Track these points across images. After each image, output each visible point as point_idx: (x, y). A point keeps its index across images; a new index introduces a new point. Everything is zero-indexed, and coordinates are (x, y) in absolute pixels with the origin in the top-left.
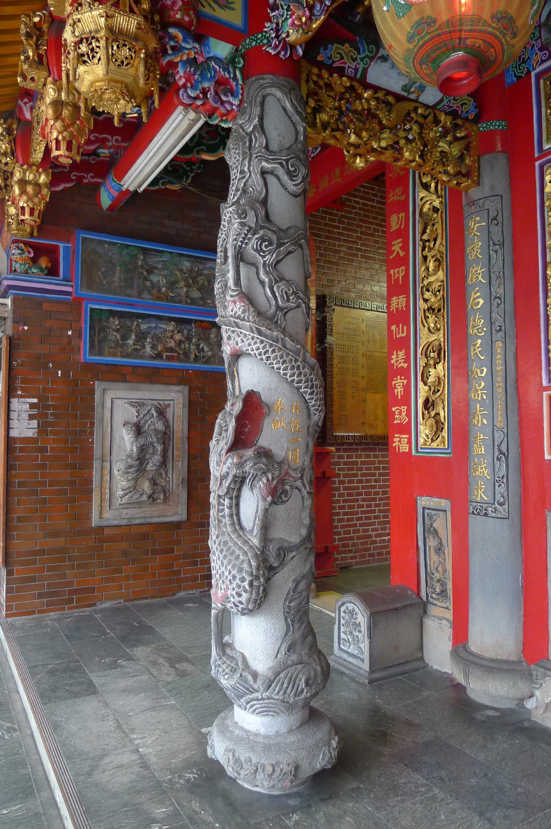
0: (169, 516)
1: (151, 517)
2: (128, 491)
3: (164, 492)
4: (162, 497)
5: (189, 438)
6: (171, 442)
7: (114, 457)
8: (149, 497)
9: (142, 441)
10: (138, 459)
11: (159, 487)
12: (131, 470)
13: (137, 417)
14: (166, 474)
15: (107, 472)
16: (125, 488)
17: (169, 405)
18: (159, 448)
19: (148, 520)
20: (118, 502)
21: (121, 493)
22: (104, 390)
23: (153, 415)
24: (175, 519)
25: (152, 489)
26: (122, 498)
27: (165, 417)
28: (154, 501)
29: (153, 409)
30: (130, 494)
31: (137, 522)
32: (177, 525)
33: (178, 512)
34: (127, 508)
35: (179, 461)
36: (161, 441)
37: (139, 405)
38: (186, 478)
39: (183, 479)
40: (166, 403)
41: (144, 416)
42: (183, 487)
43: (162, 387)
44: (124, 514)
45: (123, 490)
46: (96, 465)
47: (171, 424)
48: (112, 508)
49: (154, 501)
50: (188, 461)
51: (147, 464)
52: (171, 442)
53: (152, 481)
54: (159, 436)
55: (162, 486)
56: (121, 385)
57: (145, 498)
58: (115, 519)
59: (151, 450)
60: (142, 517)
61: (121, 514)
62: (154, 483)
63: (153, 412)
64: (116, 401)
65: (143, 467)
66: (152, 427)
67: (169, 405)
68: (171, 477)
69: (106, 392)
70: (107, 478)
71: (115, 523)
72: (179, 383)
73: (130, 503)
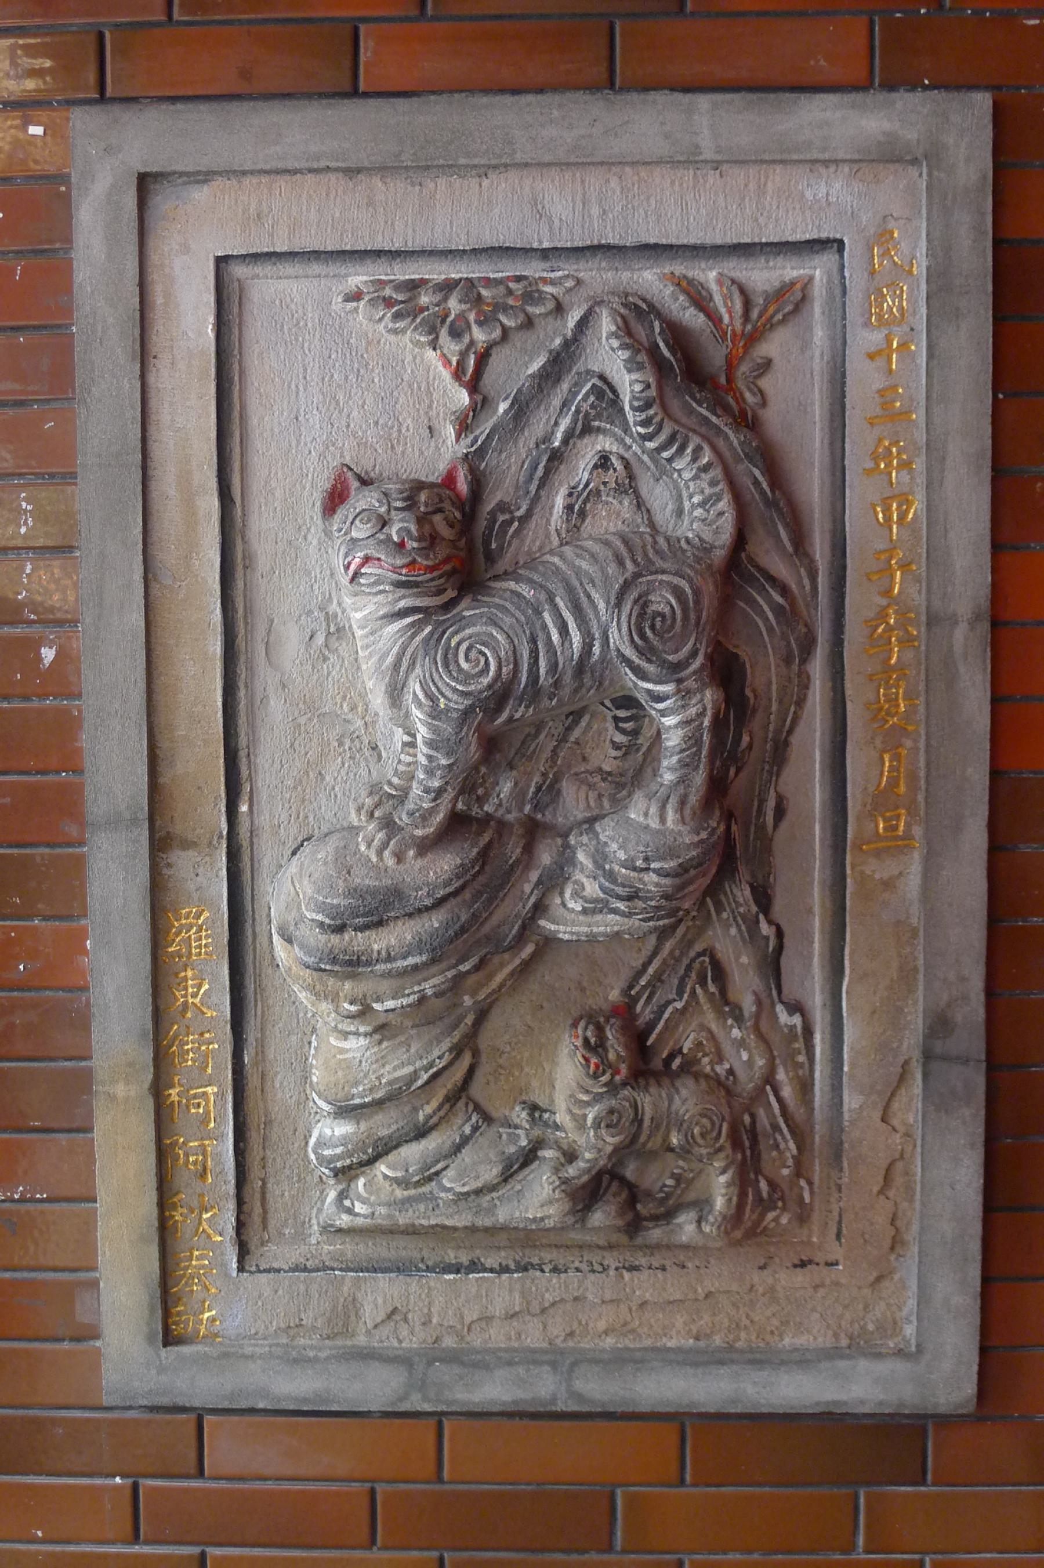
0: (803, 1360)
1: (621, 1361)
2: (391, 1119)
3: (746, 1146)
4: (719, 1187)
5: (1000, 621)
6: (818, 668)
7: (271, 807)
8: (585, 1196)
9: (486, 639)
10: (457, 825)
11: (686, 1100)
12: (379, 941)
13: (464, 425)
14: (772, 966)
15: (201, 932)
16: (360, 1095)
17: (791, 301)
18: (674, 721)
19: (598, 1389)
20: (321, 1212)
21: (331, 1133)
22: (145, 183)
23: (606, 392)
24: (863, 1387)
25: (609, 1121)
26: (345, 1174)
27: (748, 421)
28: (634, 1226)
29: (606, 324)
30: (413, 1152)
31: (494, 1391)
32: (891, 1444)
33: (890, 1327)
34: (401, 1268)
35: (896, 845)
36: (692, 651)
37: (476, 308)
38: (973, 1010)
39: (940, 1025)
40: (762, 276)
41: (521, 411)
42: (938, 1101)
43: (711, 120)
44: (371, 1310)
45: (344, 1111)
46: (113, 873)
47: (812, 487)
48: (278, 1253)
49: (634, 1226)
50: (996, 848)
51: (555, 879)
52: (818, 668)
53: (616, 1046)
54: (662, 601)
55: (723, 1086)
56: (301, 129)
57: (538, 1198)
58: (300, 1361)
59: (602, 743)
60: (532, 1358)
61: (351, 1309)
62: (635, 1053)
63: (609, 357)
64: (268, 290)
65: (511, 909)
66: (612, 517)
67: (791, 301)
68: (817, 1001)
69: (162, 202)
70: (205, 990)
71: (294, 1387)
72: (895, 64)
73: (412, 1231)
